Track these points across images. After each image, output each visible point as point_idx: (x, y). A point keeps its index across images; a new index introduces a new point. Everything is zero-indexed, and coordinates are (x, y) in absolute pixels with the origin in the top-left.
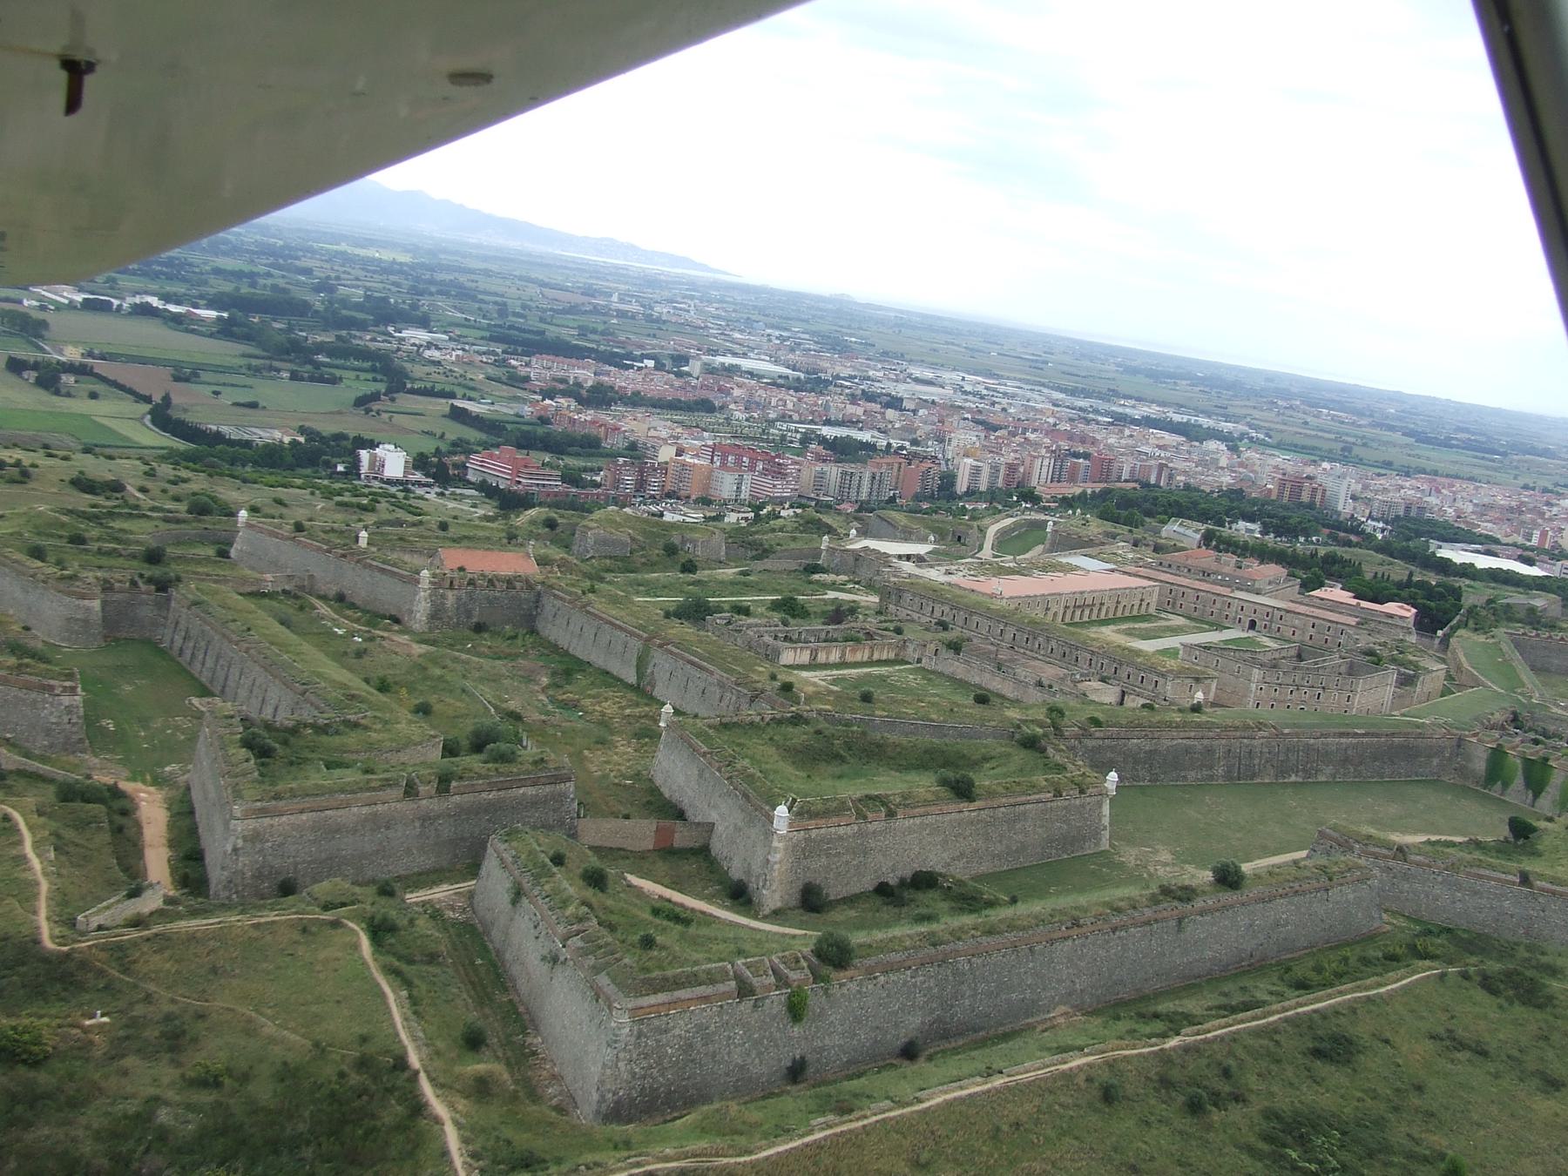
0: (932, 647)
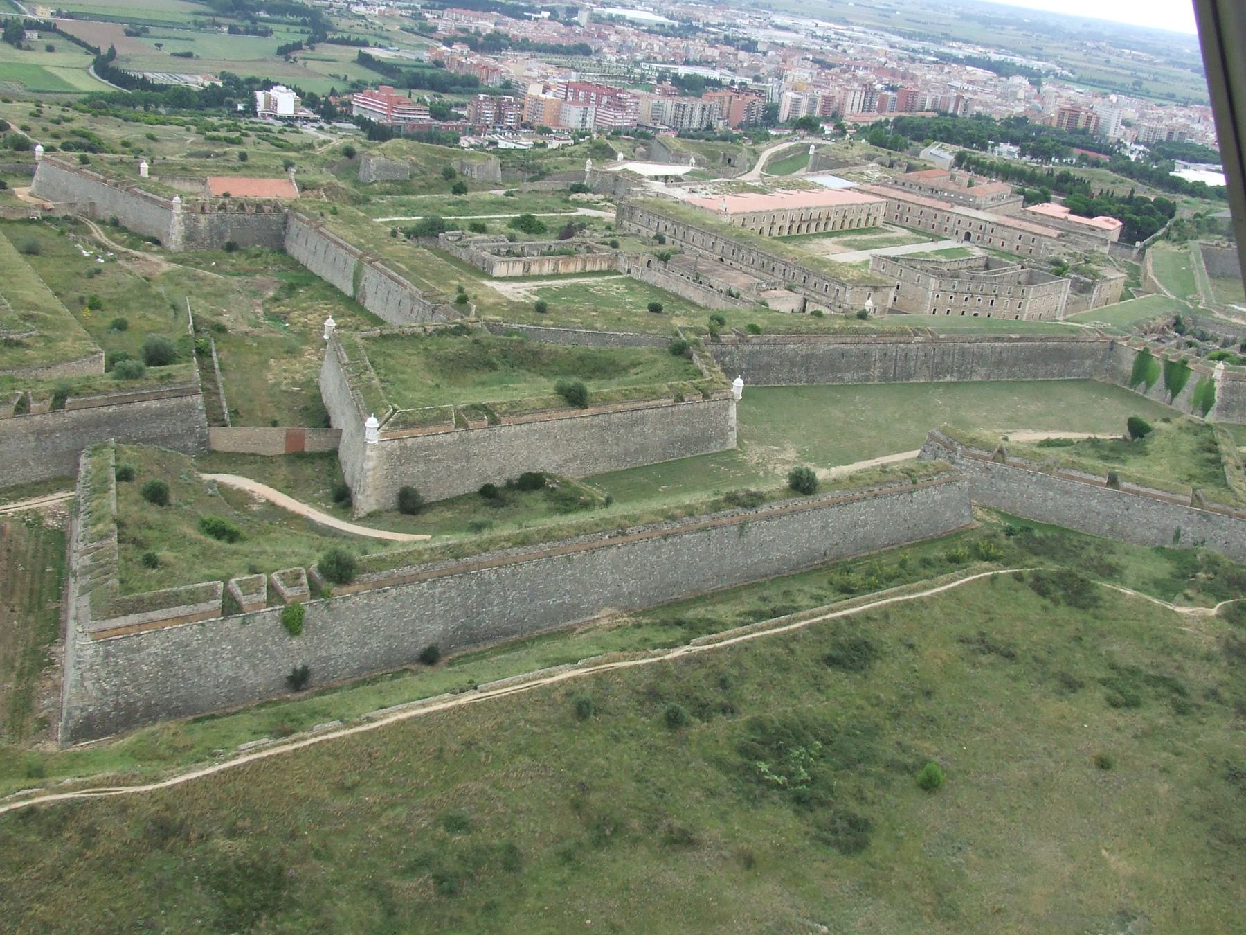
0: (644, 259)
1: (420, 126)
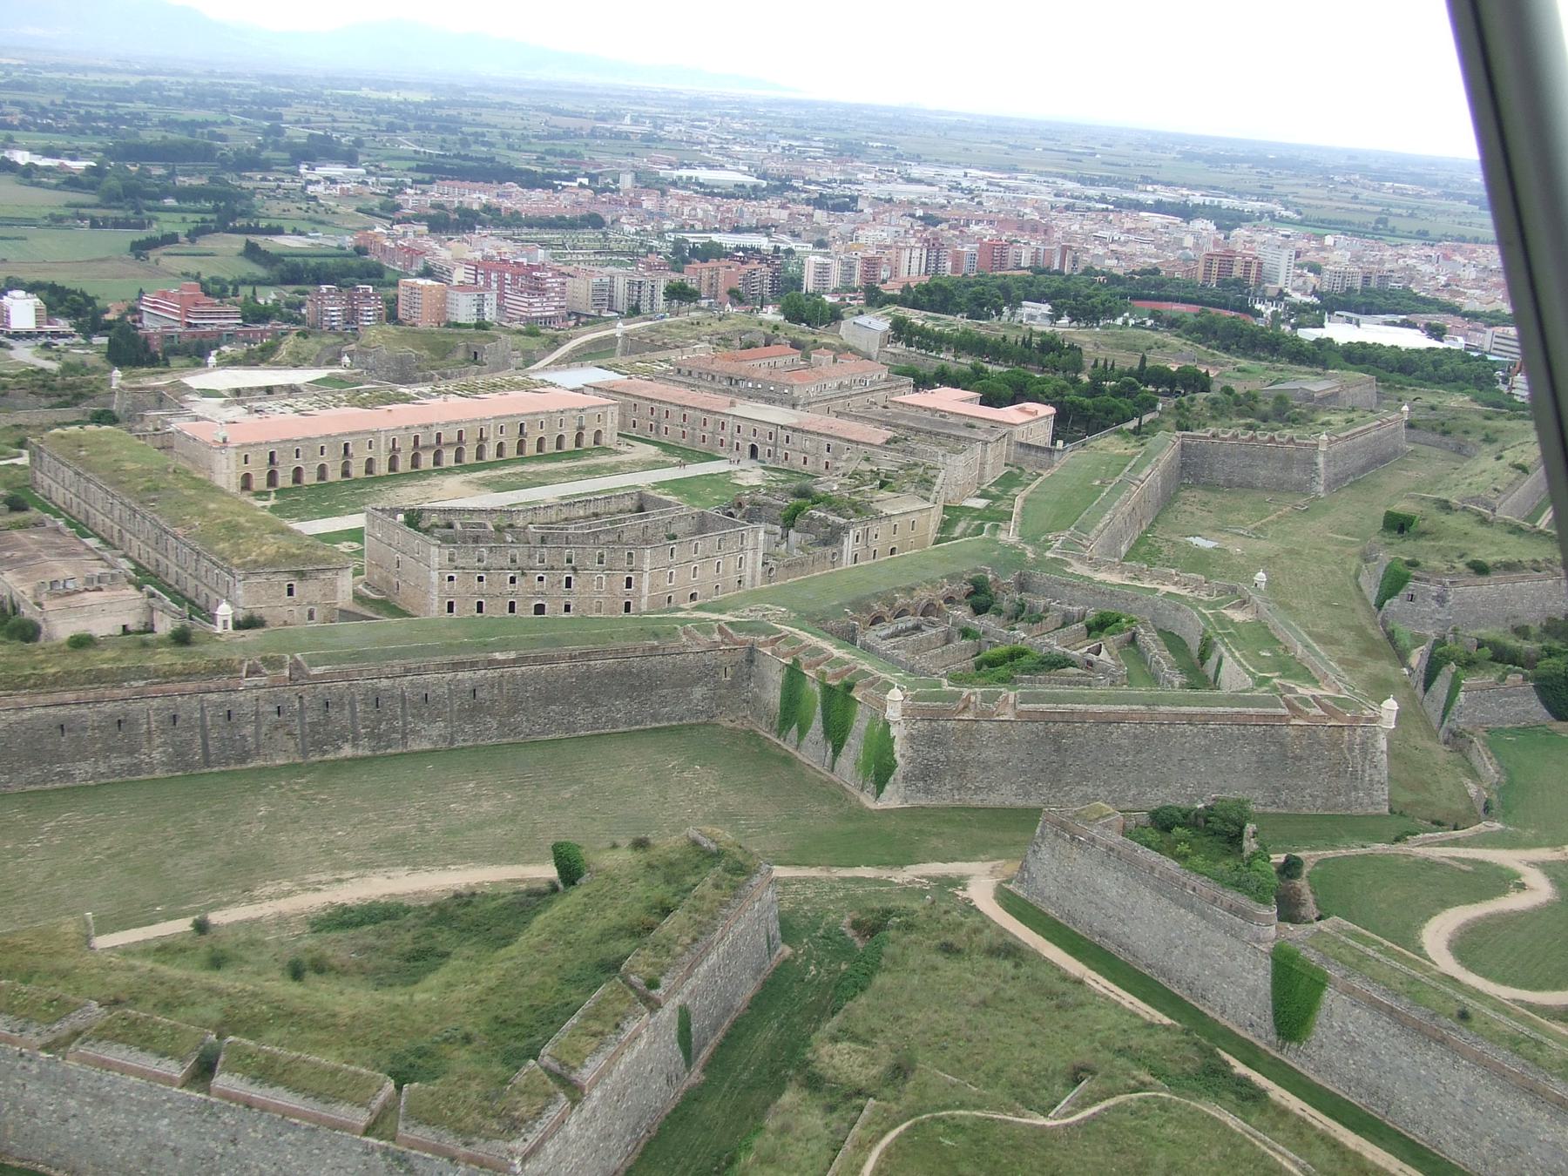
1: (204, 335)
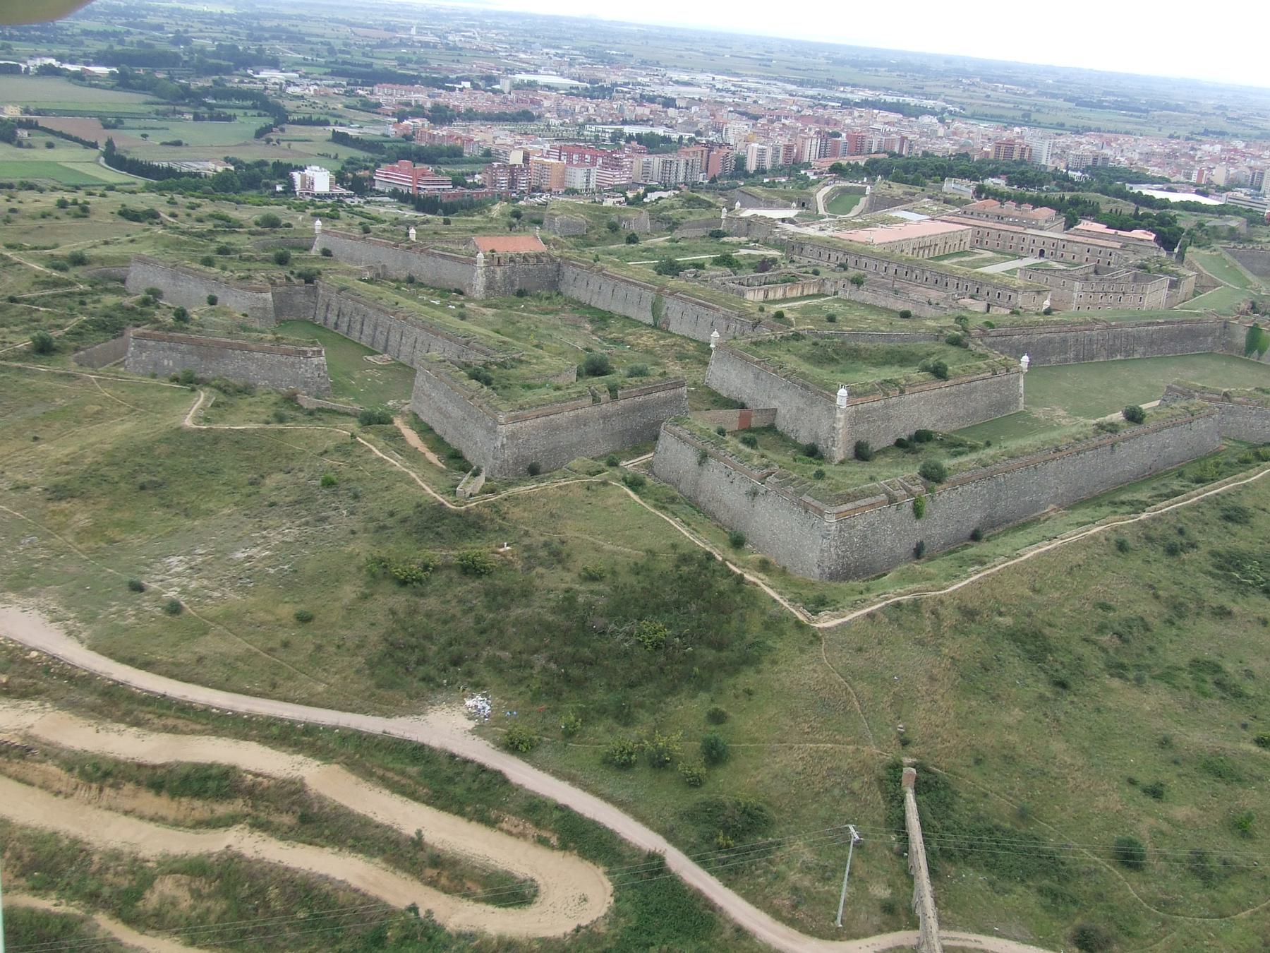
0: (841, 283)
